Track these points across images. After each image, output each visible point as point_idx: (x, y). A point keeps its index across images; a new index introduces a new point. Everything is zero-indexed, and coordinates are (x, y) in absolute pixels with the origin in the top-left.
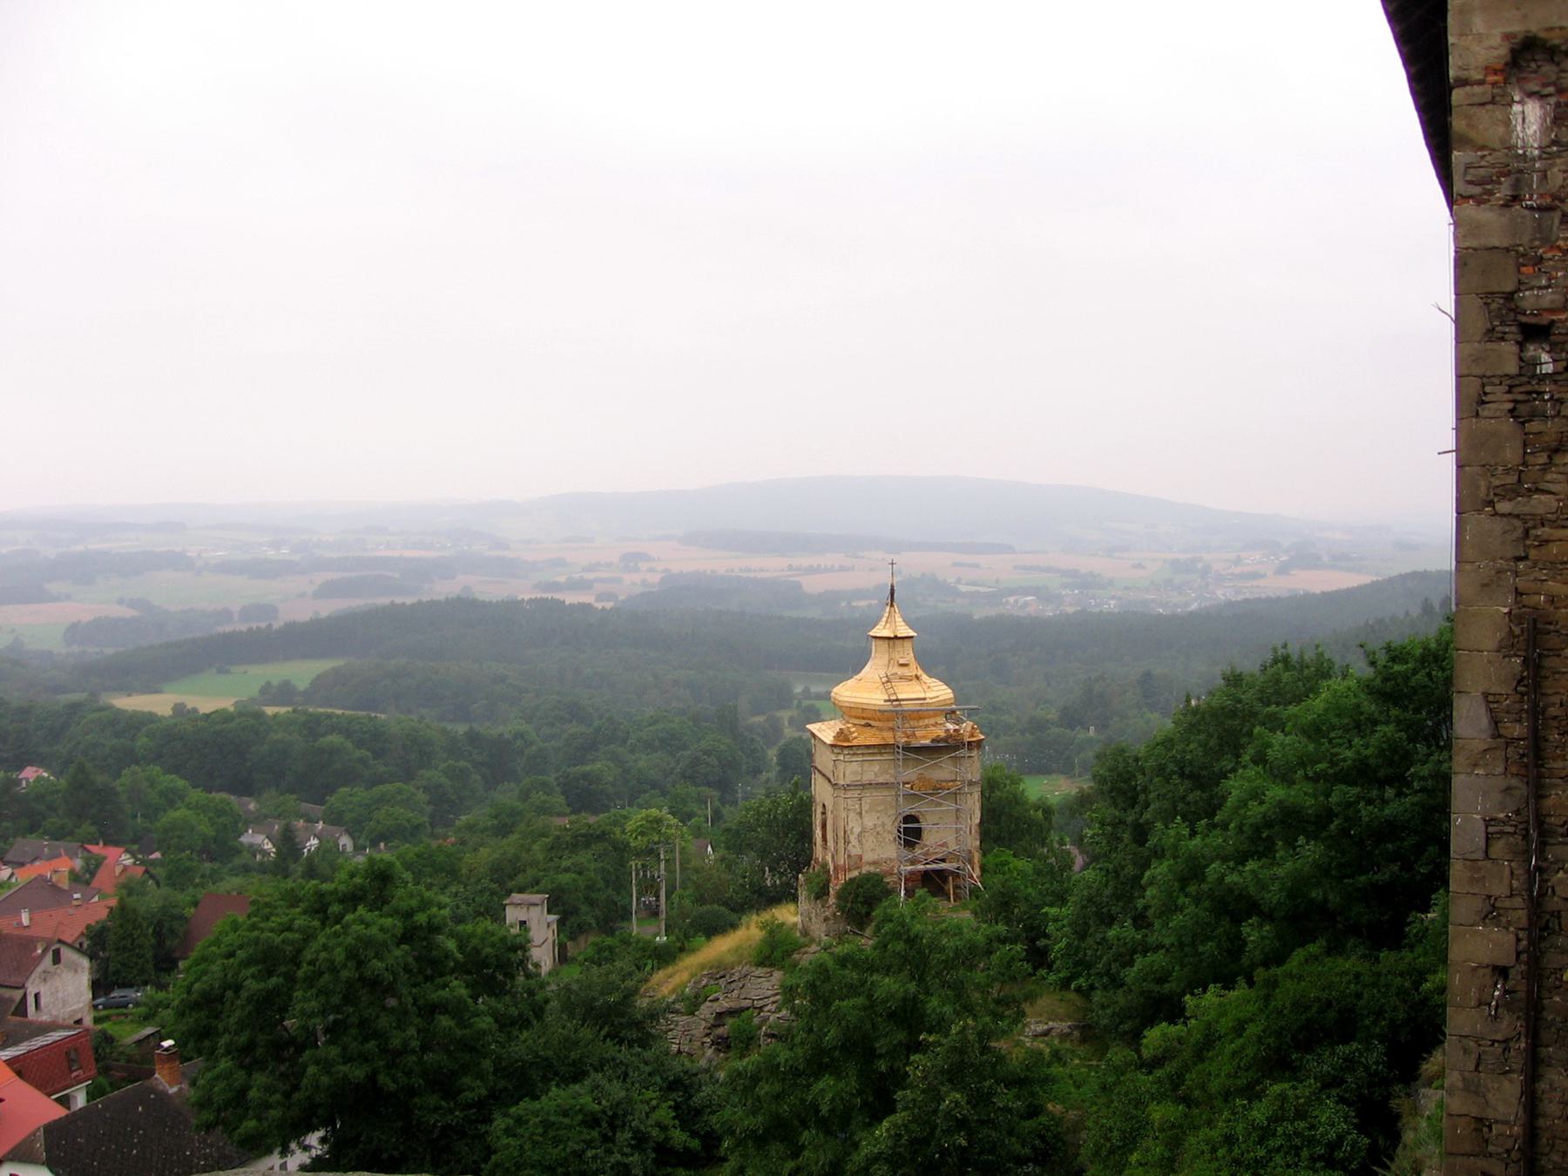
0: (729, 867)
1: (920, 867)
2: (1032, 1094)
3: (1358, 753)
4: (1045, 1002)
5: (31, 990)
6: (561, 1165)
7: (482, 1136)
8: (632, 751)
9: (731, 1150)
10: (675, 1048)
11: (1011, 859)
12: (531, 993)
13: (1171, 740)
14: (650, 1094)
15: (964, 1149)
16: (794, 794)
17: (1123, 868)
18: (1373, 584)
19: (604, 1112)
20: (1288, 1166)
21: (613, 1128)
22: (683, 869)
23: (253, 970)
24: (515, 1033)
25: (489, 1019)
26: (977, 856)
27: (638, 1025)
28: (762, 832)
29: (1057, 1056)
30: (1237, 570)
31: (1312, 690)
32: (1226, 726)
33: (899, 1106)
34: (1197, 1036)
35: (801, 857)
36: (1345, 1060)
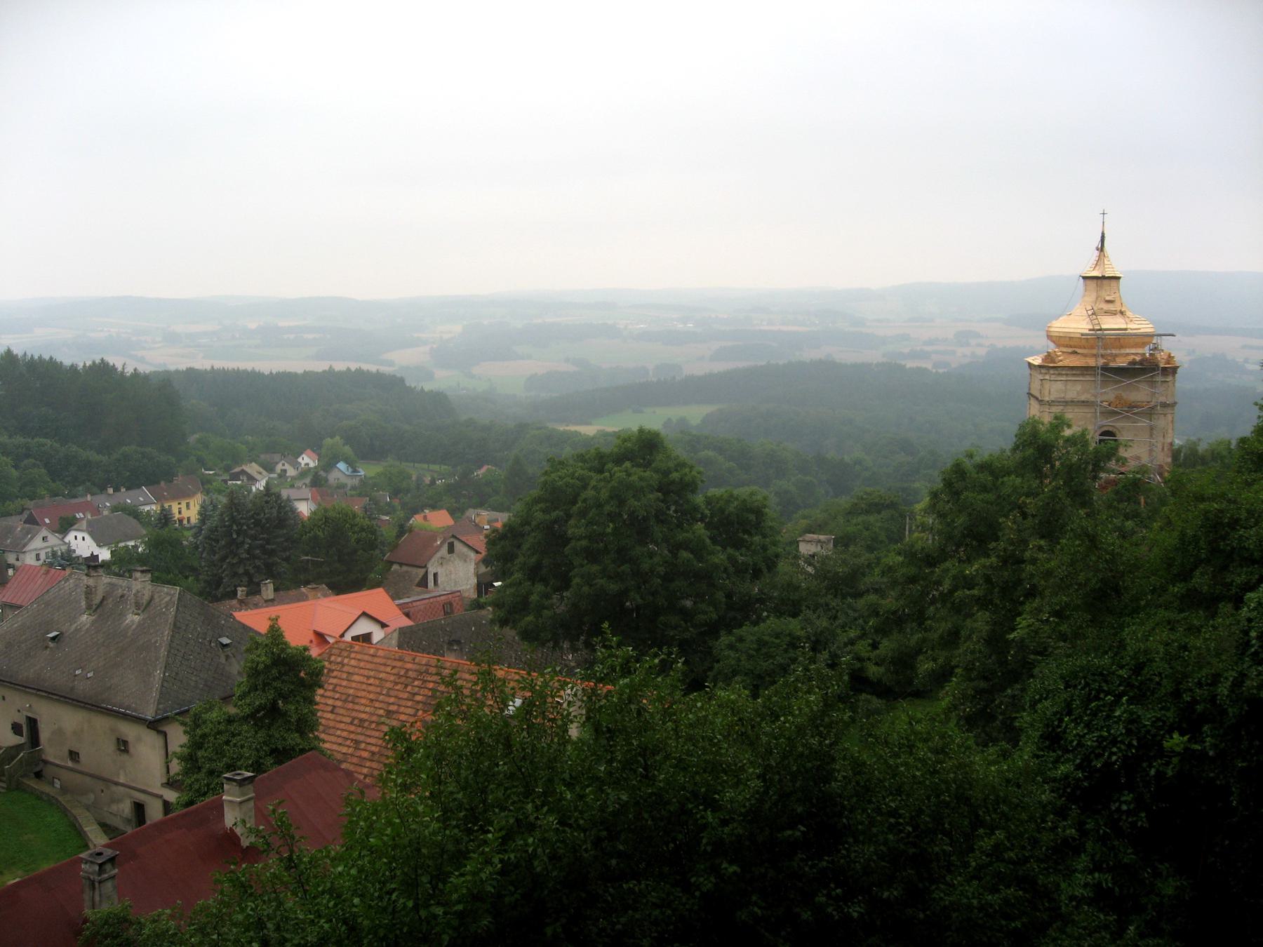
5: (431, 570)
6: (769, 675)
12: (764, 548)
23: (542, 505)
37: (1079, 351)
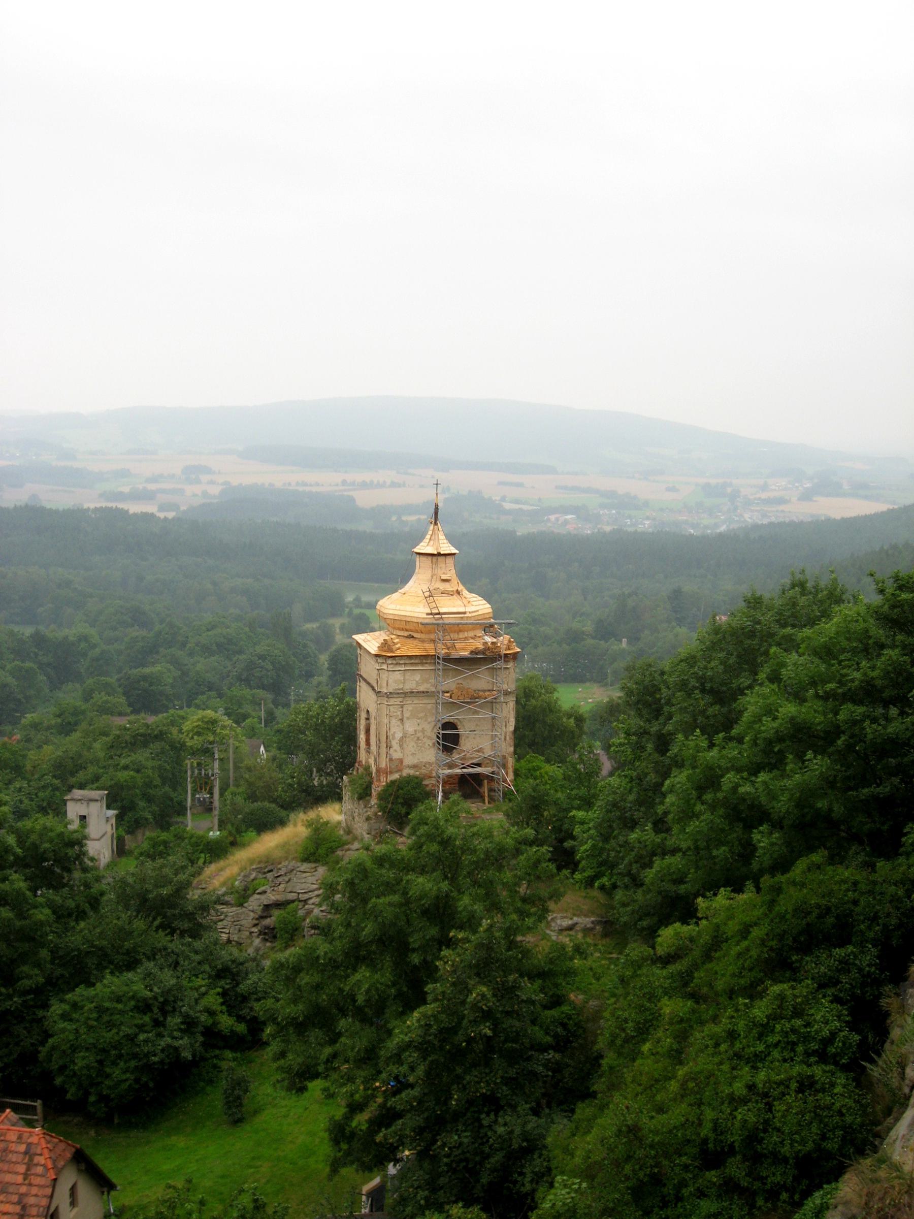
0: (280, 767)
1: (458, 771)
2: (556, 985)
3: (865, 674)
4: (572, 898)
6: (115, 1048)
7: (39, 1021)
8: (191, 654)
9: (274, 1037)
10: (224, 937)
11: (543, 765)
12: (87, 886)
13: (693, 657)
14: (199, 982)
15: (489, 1039)
16: (341, 700)
17: (646, 775)
18: (890, 511)
19: (155, 998)
20: (785, 1060)
21: (164, 1013)
22: (237, 768)
24: (73, 924)
25: (47, 911)
26: (511, 762)
27: (190, 916)
28: (310, 735)
29: (579, 950)
30: (764, 496)
31: (826, 614)
32: (746, 646)
33: (430, 998)
34: (706, 938)
35: (346, 760)
36: (840, 962)
37: (415, 635)
